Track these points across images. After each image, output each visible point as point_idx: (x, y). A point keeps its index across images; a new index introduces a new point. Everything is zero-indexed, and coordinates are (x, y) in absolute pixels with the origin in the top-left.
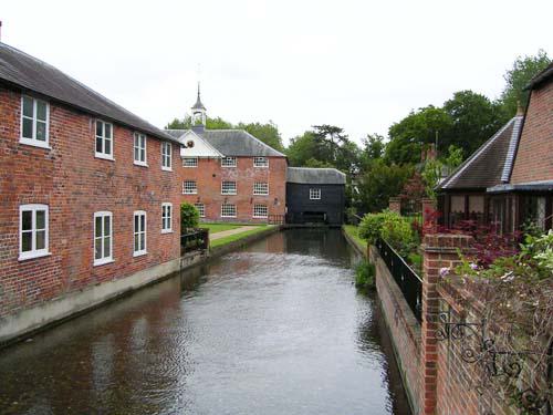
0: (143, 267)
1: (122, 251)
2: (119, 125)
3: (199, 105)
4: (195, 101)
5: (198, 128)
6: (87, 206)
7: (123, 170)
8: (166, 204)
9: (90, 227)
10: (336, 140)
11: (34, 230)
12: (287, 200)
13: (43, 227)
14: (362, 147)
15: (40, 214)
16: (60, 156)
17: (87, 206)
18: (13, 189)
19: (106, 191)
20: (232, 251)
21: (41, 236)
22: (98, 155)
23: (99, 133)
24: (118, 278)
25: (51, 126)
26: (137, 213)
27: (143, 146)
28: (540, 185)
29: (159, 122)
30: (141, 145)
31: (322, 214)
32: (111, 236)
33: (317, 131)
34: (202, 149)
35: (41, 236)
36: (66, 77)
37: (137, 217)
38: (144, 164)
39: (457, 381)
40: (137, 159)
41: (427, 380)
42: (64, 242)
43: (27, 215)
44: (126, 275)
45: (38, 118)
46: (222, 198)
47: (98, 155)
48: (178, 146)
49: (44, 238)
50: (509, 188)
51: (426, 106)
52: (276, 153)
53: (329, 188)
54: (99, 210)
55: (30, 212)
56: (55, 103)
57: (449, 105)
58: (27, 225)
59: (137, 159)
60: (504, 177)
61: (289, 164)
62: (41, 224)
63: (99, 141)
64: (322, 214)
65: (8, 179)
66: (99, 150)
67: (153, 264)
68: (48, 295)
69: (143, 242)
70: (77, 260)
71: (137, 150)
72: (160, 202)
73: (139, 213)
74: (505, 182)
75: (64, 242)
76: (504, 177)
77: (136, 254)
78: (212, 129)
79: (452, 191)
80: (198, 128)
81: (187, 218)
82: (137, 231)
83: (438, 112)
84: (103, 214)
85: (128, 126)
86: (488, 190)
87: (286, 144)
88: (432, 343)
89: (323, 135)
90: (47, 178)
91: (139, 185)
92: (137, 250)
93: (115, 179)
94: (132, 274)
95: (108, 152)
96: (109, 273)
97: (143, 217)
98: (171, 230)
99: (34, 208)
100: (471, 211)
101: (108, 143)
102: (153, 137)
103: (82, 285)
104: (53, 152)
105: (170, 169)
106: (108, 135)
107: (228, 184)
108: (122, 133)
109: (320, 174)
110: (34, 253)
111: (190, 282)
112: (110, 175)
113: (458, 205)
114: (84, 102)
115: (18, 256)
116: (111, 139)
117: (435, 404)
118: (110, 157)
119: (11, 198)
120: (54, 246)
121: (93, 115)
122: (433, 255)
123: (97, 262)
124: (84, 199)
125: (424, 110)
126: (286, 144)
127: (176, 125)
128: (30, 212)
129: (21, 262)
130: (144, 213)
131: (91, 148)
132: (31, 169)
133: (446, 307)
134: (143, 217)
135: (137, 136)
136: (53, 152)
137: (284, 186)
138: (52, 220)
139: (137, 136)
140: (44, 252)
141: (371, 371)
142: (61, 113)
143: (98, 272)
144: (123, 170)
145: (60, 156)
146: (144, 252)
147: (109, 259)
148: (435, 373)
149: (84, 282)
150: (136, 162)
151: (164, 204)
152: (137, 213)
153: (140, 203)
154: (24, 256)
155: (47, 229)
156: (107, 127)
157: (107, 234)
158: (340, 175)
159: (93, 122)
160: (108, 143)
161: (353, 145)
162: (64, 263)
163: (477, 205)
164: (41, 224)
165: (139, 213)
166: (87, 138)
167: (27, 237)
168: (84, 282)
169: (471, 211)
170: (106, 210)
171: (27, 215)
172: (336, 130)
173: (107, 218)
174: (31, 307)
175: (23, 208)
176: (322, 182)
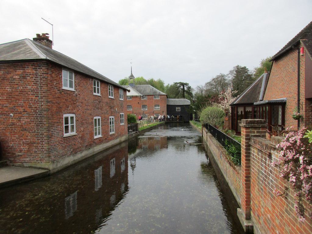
0: (114, 139)
1: (105, 132)
5: (132, 85)
7: (105, 100)
8: (122, 114)
9: (92, 123)
11: (70, 125)
17: (91, 115)
19: (98, 108)
21: (72, 127)
22: (94, 94)
23: (95, 85)
28: (277, 100)
29: (116, 79)
30: (111, 89)
32: (100, 126)
34: (133, 93)
35: (72, 127)
38: (113, 97)
42: (82, 129)
43: (67, 119)
44: (107, 142)
45: (95, 88)
46: (142, 112)
47: (94, 94)
48: (125, 90)
49: (97, 130)
50: (262, 102)
54: (95, 116)
55: (96, 119)
58: (67, 122)
59: (110, 95)
60: (260, 98)
61: (167, 98)
62: (72, 122)
63: (95, 88)
66: (95, 92)
67: (117, 138)
68: (75, 152)
69: (113, 128)
70: (87, 137)
72: (119, 113)
74: (261, 100)
75: (82, 129)
76: (260, 98)
77: (111, 133)
78: (138, 83)
79: (238, 105)
81: (131, 120)
84: (97, 118)
85: (105, 82)
86: (255, 103)
90: (74, 103)
91: (111, 105)
92: (111, 132)
94: (109, 142)
96: (100, 141)
98: (124, 124)
99: (69, 116)
100: (246, 111)
101: (98, 89)
102: (116, 87)
103: (89, 146)
105: (123, 100)
107: (144, 106)
108: (103, 85)
110: (70, 134)
111: (132, 146)
112: (100, 102)
113: (240, 110)
114: (72, 65)
115: (63, 135)
116: (99, 88)
117: (250, 195)
118: (99, 95)
119: (60, 111)
120: (78, 131)
121: (92, 78)
123: (95, 137)
124: (89, 112)
127: (124, 82)
129: (64, 138)
131: (92, 91)
135: (110, 86)
136: (76, 93)
137: (166, 106)
138: (77, 120)
139: (110, 86)
140: (74, 133)
141: (212, 193)
142: (78, 76)
143: (96, 141)
144: (105, 100)
146: (114, 133)
147: (100, 136)
148: (250, 181)
149: (91, 145)
150: (110, 97)
151: (121, 113)
153: (112, 113)
154: (66, 135)
155: (75, 124)
157: (99, 125)
159: (92, 81)
160: (98, 89)
163: (249, 109)
164: (72, 122)
166: (90, 87)
167: (67, 128)
169: (246, 111)
171: (67, 119)
173: (99, 119)
175: (65, 116)
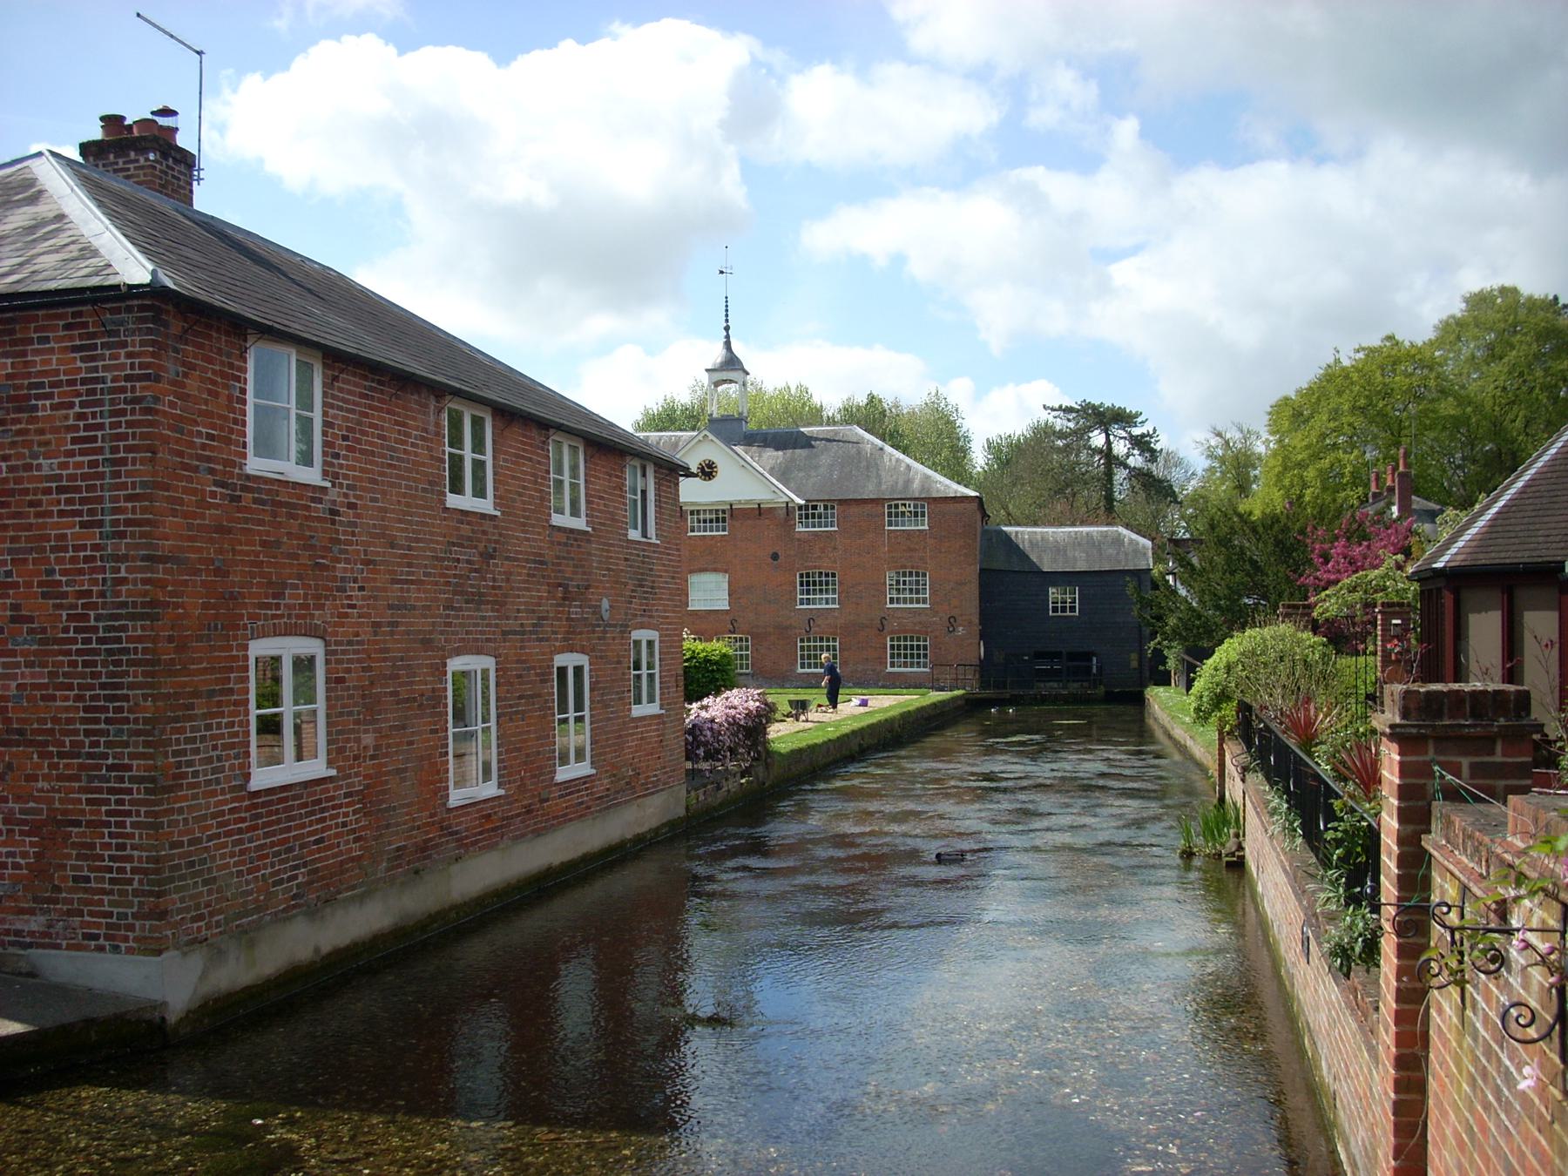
0: (582, 812)
2: (507, 416)
3: (731, 363)
4: (716, 354)
5: (731, 429)
6: (427, 643)
9: (437, 698)
10: (1120, 448)
12: (985, 617)
13: (312, 701)
14: (1199, 463)
15: (304, 665)
16: (352, 506)
17: (427, 643)
18: (233, 597)
19: (477, 600)
20: (852, 758)
22: (453, 501)
24: (516, 838)
25: (326, 424)
26: (560, 660)
27: (478, 446)
31: (1087, 656)
33: (1060, 424)
34: (743, 480)
36: (305, 259)
37: (562, 671)
38: (580, 524)
39: (1487, 1106)
40: (457, 488)
41: (1398, 1108)
44: (538, 833)
45: (461, 458)
47: (453, 501)
51: (1375, 341)
52: (948, 486)
53: (1101, 586)
55: (277, 660)
56: (337, 360)
57: (1452, 331)
62: (304, 692)
63: (457, 462)
64: (1087, 656)
65: (217, 572)
68: (324, 891)
71: (559, 483)
72: (625, 630)
73: (568, 660)
75: (368, 739)
80: (731, 429)
82: (563, 710)
83: (1418, 358)
87: (979, 459)
88: (1413, 998)
89: (1081, 433)
93: (499, 566)
95: (479, 492)
96: (489, 826)
97: (578, 670)
101: (479, 466)
102: (605, 446)
103: (418, 859)
104: (334, 494)
106: (478, 446)
108: (517, 437)
109: (1077, 542)
112: (487, 556)
115: (247, 777)
118: (486, 506)
120: (341, 750)
121: (440, 391)
122: (1100, 729)
125: (1371, 351)
126: (979, 459)
127: (667, 419)
128: (277, 660)
129: (257, 794)
130: (582, 660)
131: (435, 482)
132: (278, 544)
133: (1452, 893)
134: (578, 670)
138: (334, 681)
140: (316, 768)
142: (351, 384)
145: (352, 506)
150: (557, 520)
152: (560, 660)
156: (477, 423)
158: (1131, 545)
160: (479, 466)
161: (1173, 461)
162: (370, 799)
165: (568, 660)
167: (271, 726)
168: (424, 849)
170: (479, 652)
172: (1121, 418)
174: (284, 917)
176: (1081, 566)
